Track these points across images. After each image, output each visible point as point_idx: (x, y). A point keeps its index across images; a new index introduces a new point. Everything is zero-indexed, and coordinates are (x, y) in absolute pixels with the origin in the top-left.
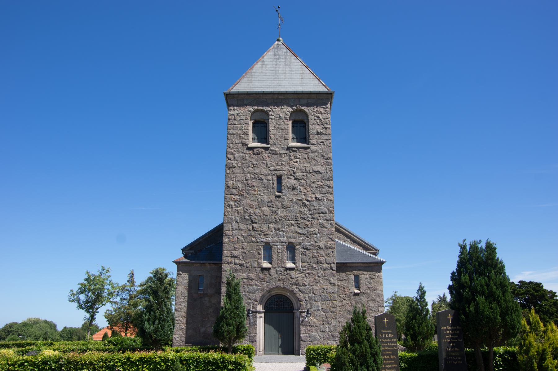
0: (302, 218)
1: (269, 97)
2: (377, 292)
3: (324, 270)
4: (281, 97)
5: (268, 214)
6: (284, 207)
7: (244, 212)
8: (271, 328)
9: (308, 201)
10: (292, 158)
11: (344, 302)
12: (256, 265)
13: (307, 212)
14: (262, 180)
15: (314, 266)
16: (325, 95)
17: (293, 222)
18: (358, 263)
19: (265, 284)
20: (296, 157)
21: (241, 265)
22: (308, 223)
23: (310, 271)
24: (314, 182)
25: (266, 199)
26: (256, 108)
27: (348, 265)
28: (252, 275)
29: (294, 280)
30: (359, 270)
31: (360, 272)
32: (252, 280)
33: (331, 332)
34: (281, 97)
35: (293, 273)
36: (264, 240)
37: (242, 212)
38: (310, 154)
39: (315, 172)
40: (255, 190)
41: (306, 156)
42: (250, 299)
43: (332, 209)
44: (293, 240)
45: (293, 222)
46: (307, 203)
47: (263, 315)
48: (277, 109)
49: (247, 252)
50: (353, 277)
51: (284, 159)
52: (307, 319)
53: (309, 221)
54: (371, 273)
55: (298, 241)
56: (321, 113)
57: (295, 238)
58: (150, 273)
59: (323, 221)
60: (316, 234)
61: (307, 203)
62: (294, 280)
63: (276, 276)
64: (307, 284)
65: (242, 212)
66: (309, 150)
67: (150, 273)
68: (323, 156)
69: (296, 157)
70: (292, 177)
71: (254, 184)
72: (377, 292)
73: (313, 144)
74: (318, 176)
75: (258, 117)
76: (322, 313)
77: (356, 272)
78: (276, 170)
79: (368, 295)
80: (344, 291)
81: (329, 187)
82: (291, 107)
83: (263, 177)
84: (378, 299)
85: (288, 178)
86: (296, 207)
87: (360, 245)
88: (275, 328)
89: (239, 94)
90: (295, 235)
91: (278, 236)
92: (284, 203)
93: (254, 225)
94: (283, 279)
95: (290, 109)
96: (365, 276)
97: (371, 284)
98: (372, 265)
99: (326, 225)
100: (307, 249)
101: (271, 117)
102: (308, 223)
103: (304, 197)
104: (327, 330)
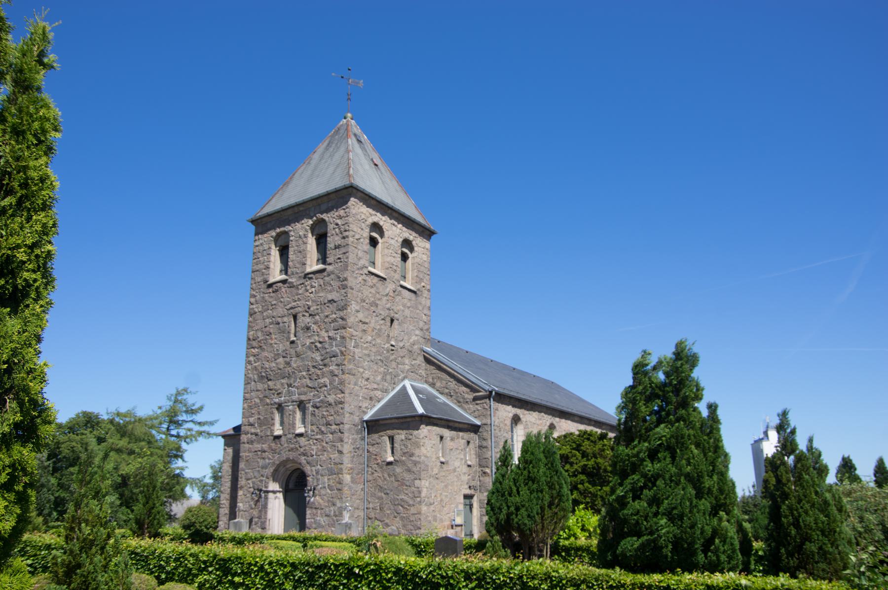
0: (314, 367)
1: (290, 212)
2: (414, 458)
3: (332, 434)
4: (301, 209)
5: (281, 366)
6: (298, 355)
7: (262, 368)
8: (291, 511)
9: (320, 342)
10: (308, 287)
11: (376, 474)
12: (269, 434)
13: (318, 358)
14: (278, 324)
15: (323, 429)
16: (344, 191)
17: (304, 373)
18: (386, 419)
19: (277, 456)
20: (312, 287)
21: (256, 435)
22: (319, 372)
23: (319, 437)
24: (327, 316)
25: (281, 347)
26: (278, 230)
27: (381, 422)
28: (265, 446)
29: (302, 450)
30: (393, 429)
31: (395, 431)
32: (265, 452)
33: (336, 516)
34: (301, 209)
35: (302, 440)
36: (277, 400)
37: (259, 368)
38: (326, 278)
39: (330, 301)
40: (271, 339)
41: (321, 282)
42: (262, 476)
43: (343, 349)
44: (303, 398)
45: (304, 373)
46: (319, 345)
47: (280, 495)
48: (298, 225)
49: (262, 418)
50: (386, 439)
51: (300, 292)
52: (312, 500)
53: (320, 369)
54: (407, 432)
55: (308, 398)
56: (340, 217)
57: (305, 394)
58: (811, 440)
59: (333, 368)
60: (326, 386)
61: (319, 345)
62: (302, 450)
63: (286, 445)
64: (314, 453)
65: (259, 368)
66: (325, 274)
67: (811, 440)
68: (339, 278)
69: (312, 287)
70: (307, 314)
71: (271, 331)
72: (414, 458)
73: (330, 264)
74: (333, 307)
75: (282, 242)
76: (328, 491)
77: (390, 432)
78: (292, 308)
79: (403, 463)
80: (376, 459)
81: (342, 319)
82: (311, 218)
83: (279, 320)
84: (414, 469)
85: (304, 316)
86: (309, 353)
87: (466, 385)
88: (295, 512)
89: (269, 215)
90: (306, 389)
91: (290, 393)
92: (298, 349)
93: (269, 383)
94: (292, 449)
95: (311, 222)
96: (401, 435)
97: (407, 447)
98: (408, 420)
99: (336, 372)
100: (317, 408)
101: (291, 238)
102: (319, 372)
103: (317, 338)
104: (332, 513)
